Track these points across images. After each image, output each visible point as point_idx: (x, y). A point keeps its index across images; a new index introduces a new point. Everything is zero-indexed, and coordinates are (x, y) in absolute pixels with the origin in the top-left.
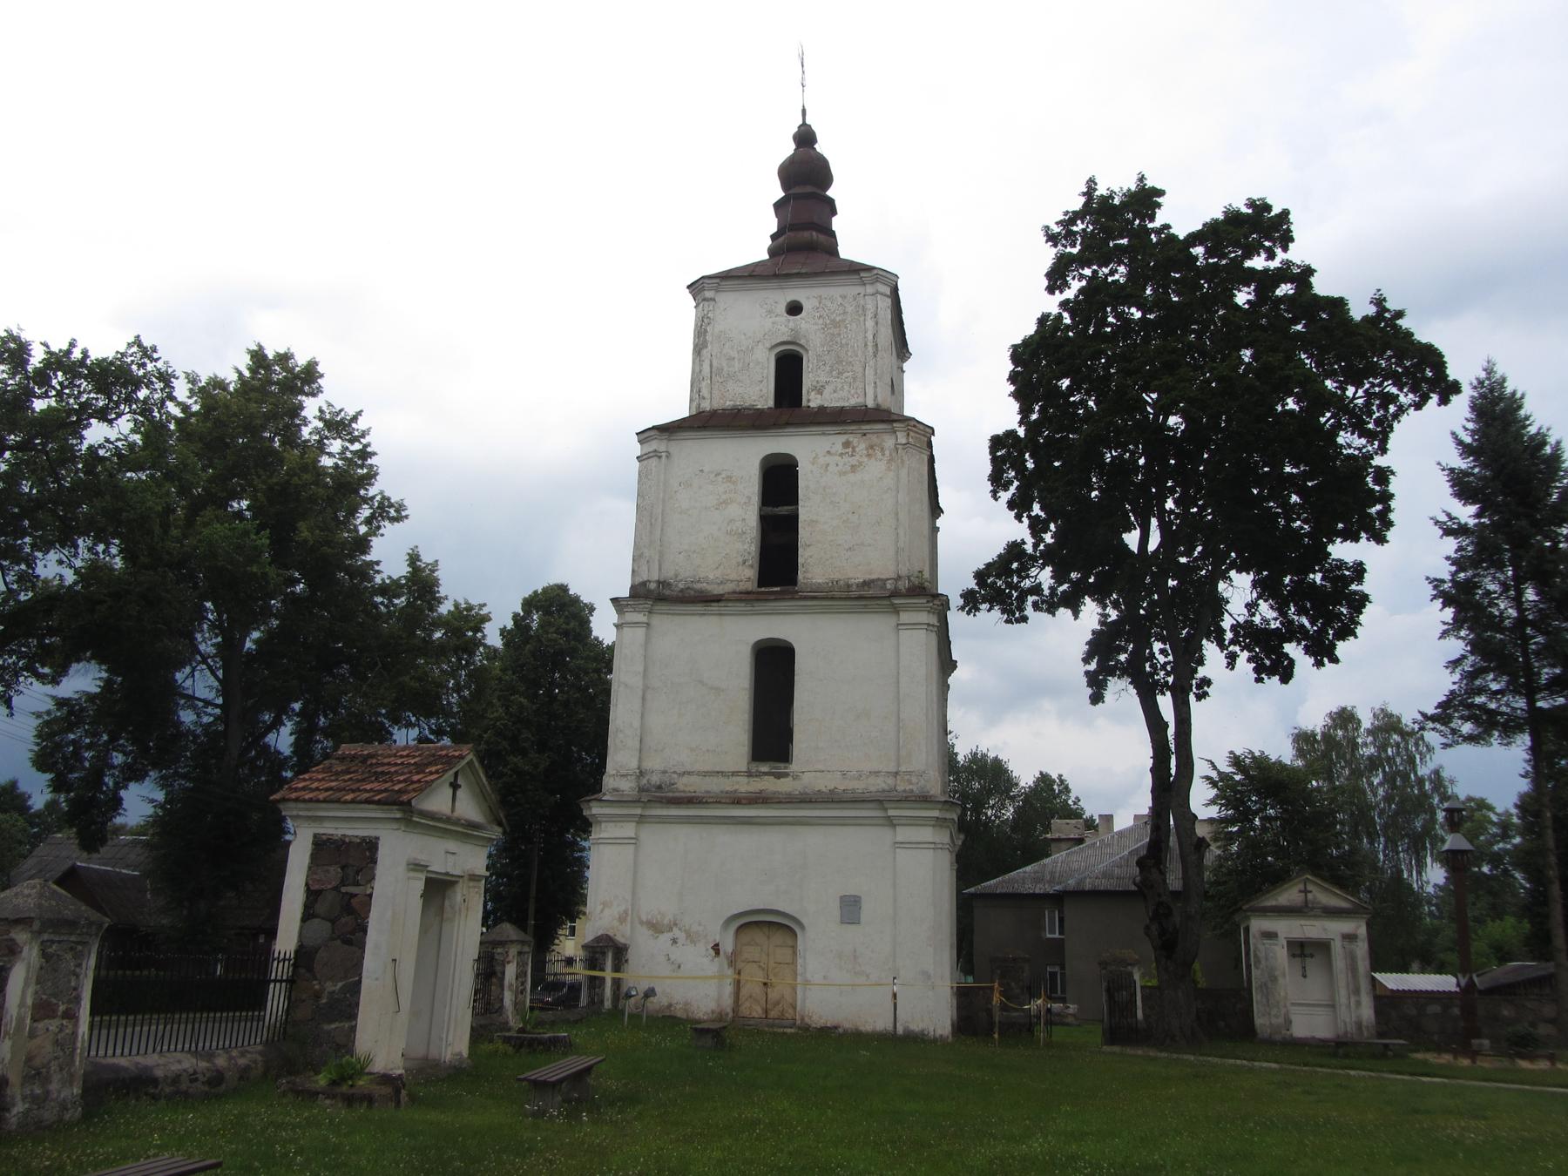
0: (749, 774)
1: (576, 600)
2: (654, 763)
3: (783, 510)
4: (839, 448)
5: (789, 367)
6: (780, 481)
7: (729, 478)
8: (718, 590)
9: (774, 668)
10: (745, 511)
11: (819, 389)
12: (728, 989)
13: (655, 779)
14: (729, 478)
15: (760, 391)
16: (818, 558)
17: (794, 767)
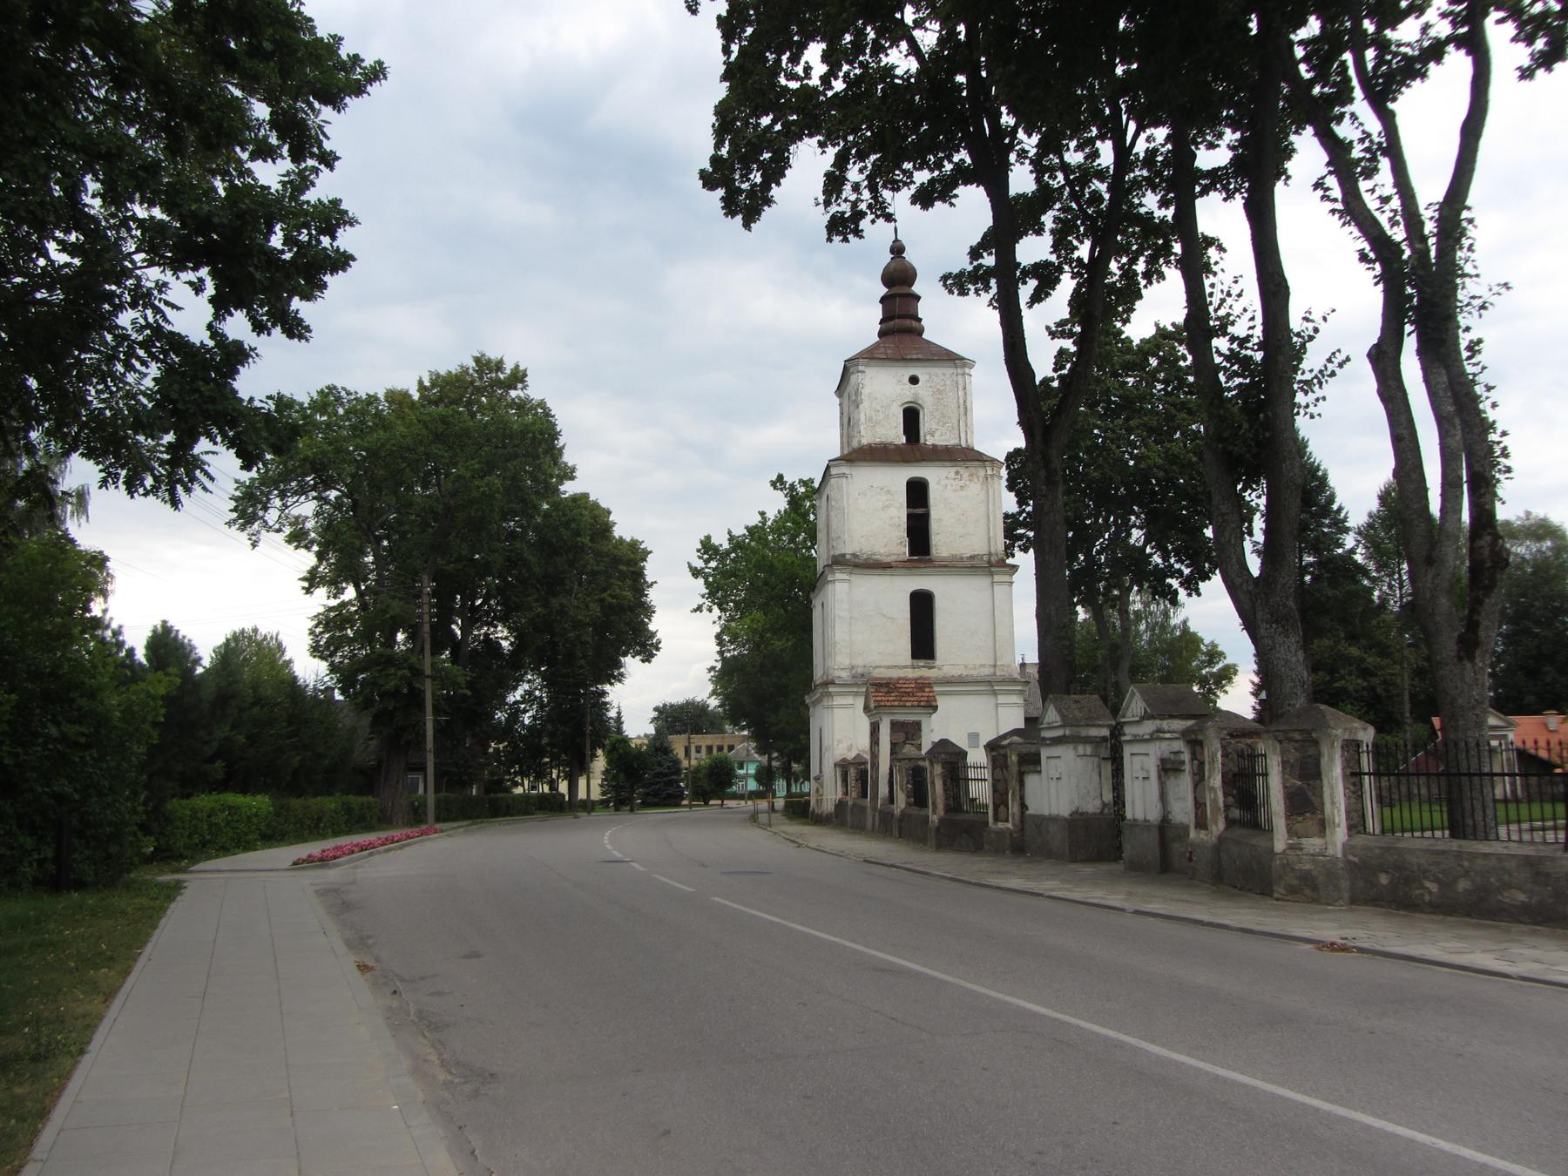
0: (913, 667)
1: (596, 505)
2: (859, 662)
3: (920, 511)
4: (952, 475)
5: (911, 417)
6: (917, 493)
7: (889, 492)
8: (888, 560)
9: (922, 605)
10: (899, 512)
11: (934, 433)
12: (1108, 797)
13: (860, 670)
14: (889, 492)
15: (895, 434)
16: (942, 541)
17: (938, 662)
